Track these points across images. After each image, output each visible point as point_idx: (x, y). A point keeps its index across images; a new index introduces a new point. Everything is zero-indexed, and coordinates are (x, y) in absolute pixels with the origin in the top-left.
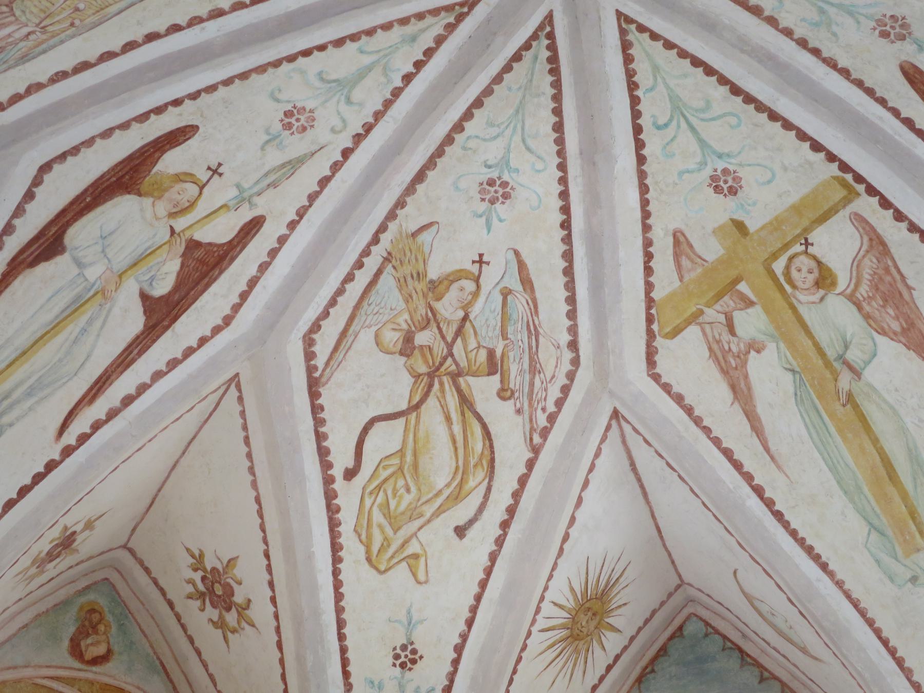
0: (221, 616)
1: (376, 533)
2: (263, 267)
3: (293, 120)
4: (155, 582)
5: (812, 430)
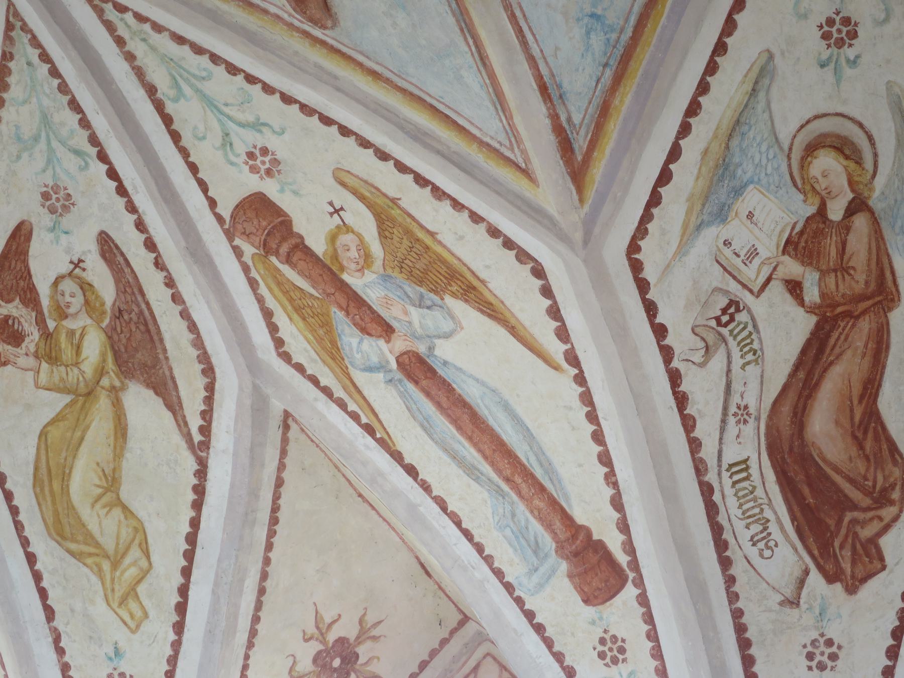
3: (609, 644)
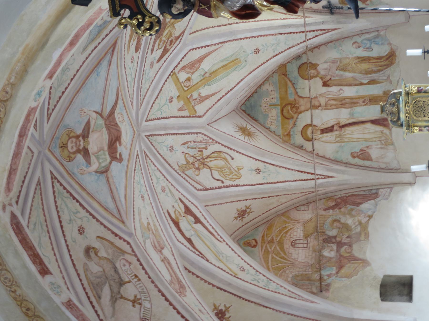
2: (187, 199)
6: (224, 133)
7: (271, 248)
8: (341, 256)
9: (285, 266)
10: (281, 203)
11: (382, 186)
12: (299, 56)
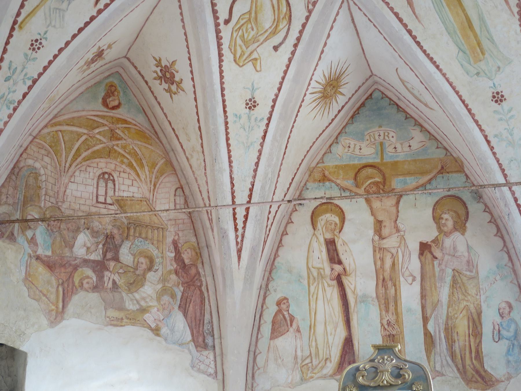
0: (169, 87)
1: (238, 48)
4: (140, 73)
5: (435, 4)
6: (329, 35)
7: (99, 133)
8: (76, 268)
9: (61, 156)
10: (189, 157)
11: (220, 358)
12: (481, 197)
